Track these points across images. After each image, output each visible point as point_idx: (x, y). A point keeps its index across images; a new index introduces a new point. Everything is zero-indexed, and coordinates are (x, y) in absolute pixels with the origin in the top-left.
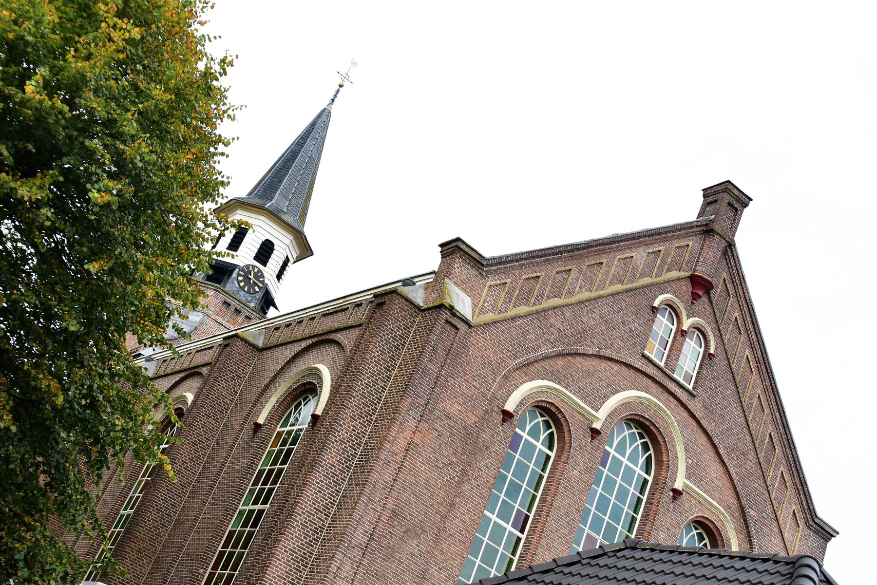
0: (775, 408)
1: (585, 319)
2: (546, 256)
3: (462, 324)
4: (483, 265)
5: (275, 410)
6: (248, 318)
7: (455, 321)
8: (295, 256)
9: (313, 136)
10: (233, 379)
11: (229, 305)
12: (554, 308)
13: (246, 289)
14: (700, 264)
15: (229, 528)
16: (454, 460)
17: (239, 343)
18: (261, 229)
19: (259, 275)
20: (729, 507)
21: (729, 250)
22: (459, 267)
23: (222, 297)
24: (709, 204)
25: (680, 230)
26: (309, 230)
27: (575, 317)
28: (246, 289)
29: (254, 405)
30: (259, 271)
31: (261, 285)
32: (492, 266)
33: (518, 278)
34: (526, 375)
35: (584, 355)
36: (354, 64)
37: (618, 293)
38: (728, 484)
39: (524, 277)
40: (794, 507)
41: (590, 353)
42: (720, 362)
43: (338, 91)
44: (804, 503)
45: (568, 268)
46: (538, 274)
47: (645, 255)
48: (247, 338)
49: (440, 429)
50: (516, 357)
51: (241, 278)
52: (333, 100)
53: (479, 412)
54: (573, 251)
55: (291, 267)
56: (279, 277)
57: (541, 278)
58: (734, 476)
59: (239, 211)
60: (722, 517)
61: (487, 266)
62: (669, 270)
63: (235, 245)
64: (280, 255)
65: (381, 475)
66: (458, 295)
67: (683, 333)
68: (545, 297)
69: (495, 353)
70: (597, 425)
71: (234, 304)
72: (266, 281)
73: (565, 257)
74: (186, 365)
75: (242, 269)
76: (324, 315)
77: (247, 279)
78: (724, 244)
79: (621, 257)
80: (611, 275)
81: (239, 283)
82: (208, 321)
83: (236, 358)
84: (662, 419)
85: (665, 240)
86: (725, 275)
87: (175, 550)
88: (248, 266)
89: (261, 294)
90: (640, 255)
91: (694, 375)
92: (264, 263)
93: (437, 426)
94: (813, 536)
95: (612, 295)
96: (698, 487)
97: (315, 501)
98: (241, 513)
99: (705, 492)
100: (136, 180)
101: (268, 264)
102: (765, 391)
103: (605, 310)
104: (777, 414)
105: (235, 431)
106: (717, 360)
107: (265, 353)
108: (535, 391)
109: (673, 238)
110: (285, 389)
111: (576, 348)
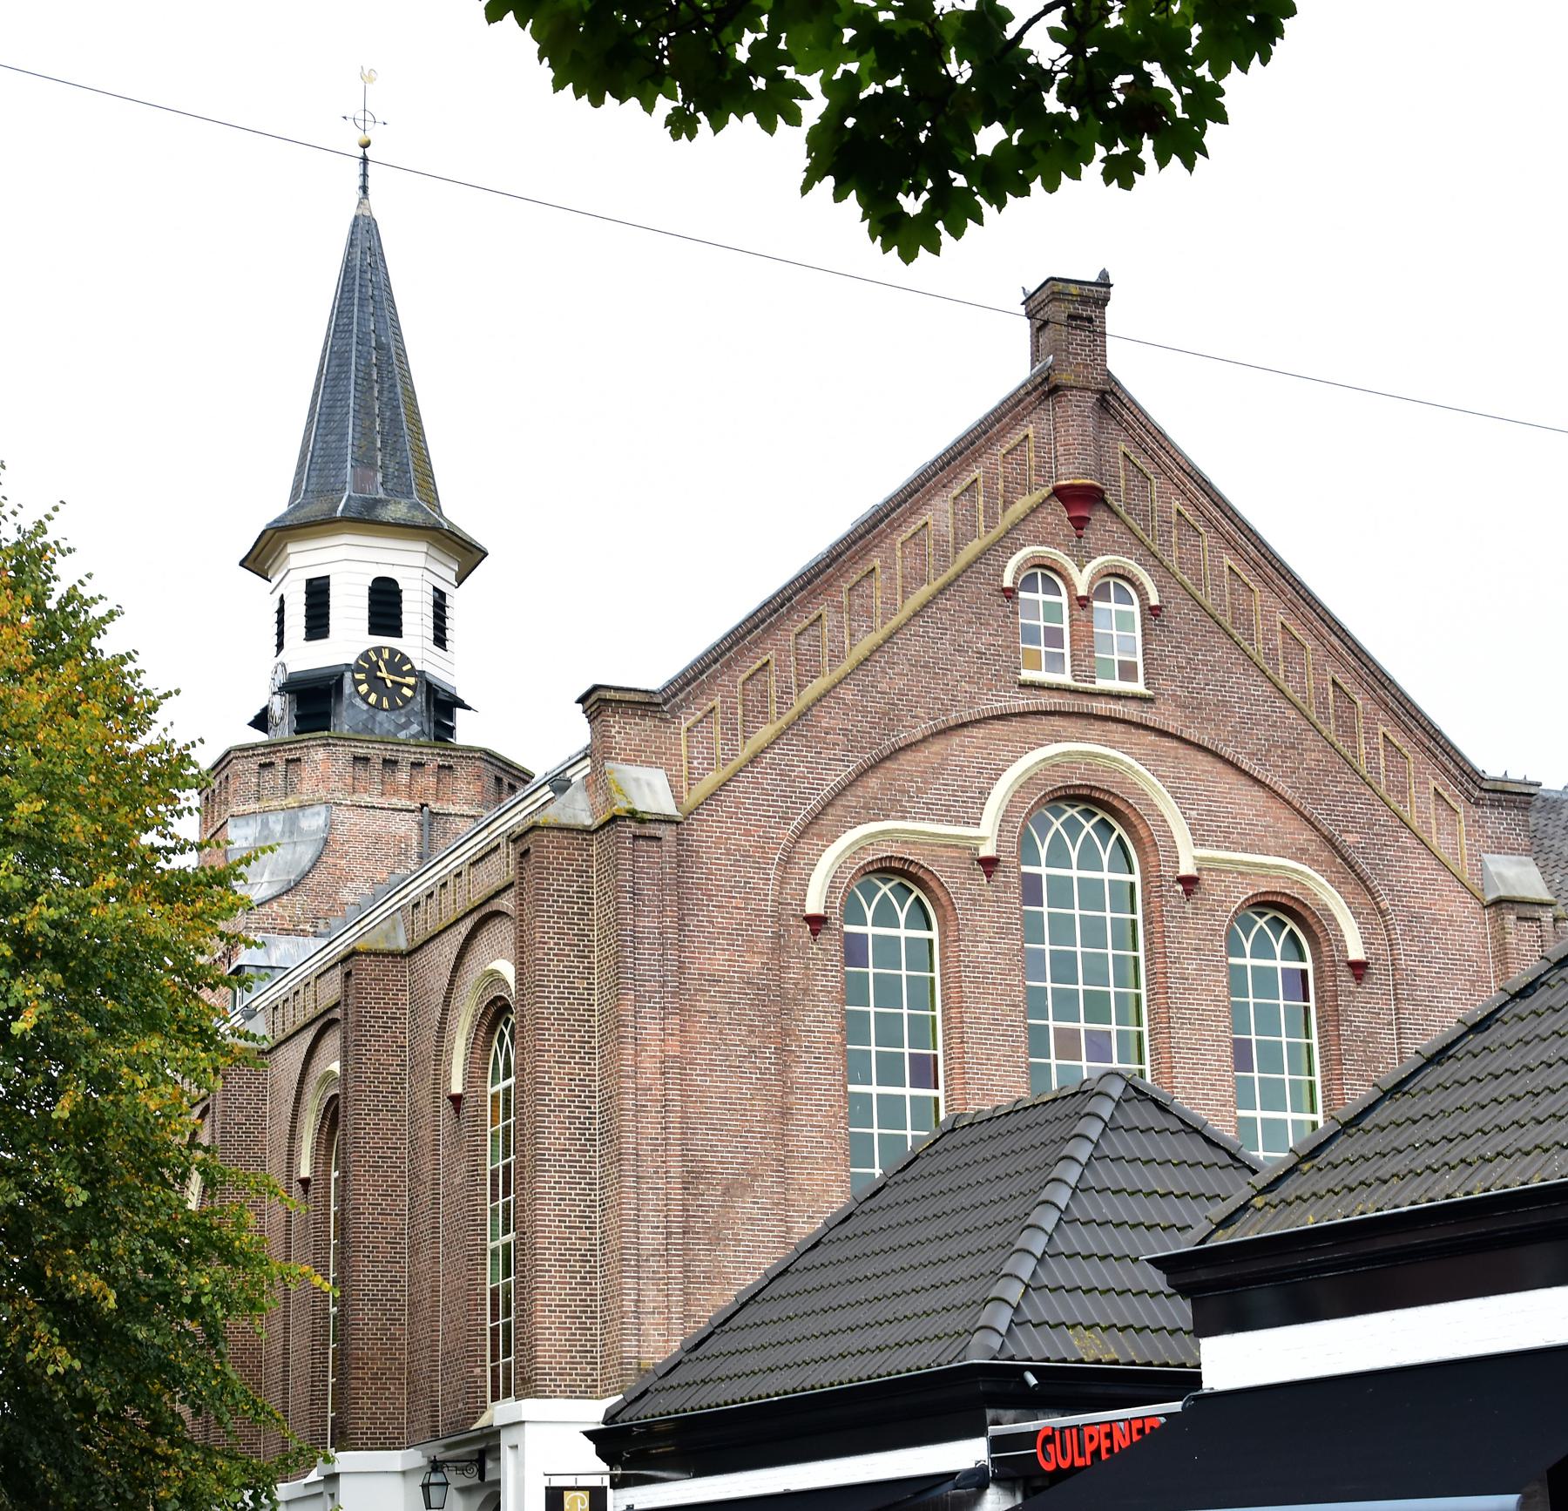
0: (1325, 630)
1: (883, 686)
2: (763, 621)
3: (663, 826)
4: (658, 705)
5: (469, 1061)
6: (417, 765)
7: (650, 830)
8: (451, 577)
10: (386, 1028)
11: (366, 760)
12: (819, 700)
13: (386, 704)
14: (1062, 459)
15: (489, 1286)
16: (755, 1042)
17: (366, 962)
18: (350, 564)
19: (398, 662)
20: (1304, 851)
21: (1110, 400)
22: (623, 730)
23: (344, 752)
24: (1039, 329)
25: (998, 420)
26: (457, 511)
27: (863, 693)
28: (386, 704)
29: (438, 1061)
31: (411, 680)
32: (675, 695)
33: (723, 694)
34: (820, 836)
35: (909, 746)
36: (367, 77)
37: (926, 605)
38: (1286, 813)
39: (740, 680)
40: (1433, 784)
41: (919, 736)
42: (1180, 611)
44: (1451, 766)
45: (813, 617)
46: (765, 659)
47: (949, 506)
48: (374, 947)
49: (708, 1007)
50: (786, 819)
51: (363, 688)
52: (364, 188)
53: (764, 944)
54: (809, 582)
55: (458, 601)
56: (440, 640)
57: (773, 662)
58: (1289, 794)
59: (291, 548)
60: (1295, 877)
61: (666, 702)
62: (1007, 504)
63: (317, 626)
65: (642, 1131)
66: (637, 780)
67: (1083, 602)
68: (795, 690)
69: (747, 833)
70: (987, 851)
71: (376, 752)
72: (418, 668)
73: (798, 603)
74: (311, 1012)
76: (473, 864)
77: (375, 683)
78: (1091, 399)
79: (905, 536)
80: (899, 581)
81: (365, 698)
82: (342, 814)
83: (374, 990)
84: (1108, 770)
85: (977, 456)
86: (1122, 447)
87: (426, 1353)
88: (365, 656)
89: (421, 699)
90: (939, 513)
91: (1139, 659)
92: (396, 631)
93: (702, 1005)
94: (1492, 815)
95: (916, 614)
96: (1227, 849)
97: (562, 1217)
98: (494, 1253)
99: (1245, 851)
100: (59, 957)
101: (405, 629)
102: (1292, 608)
103: (915, 647)
104: (1333, 639)
105: (429, 1118)
106: (1171, 609)
107: (417, 957)
108: (848, 854)
109: (991, 442)
110: (469, 1019)
111: (887, 744)
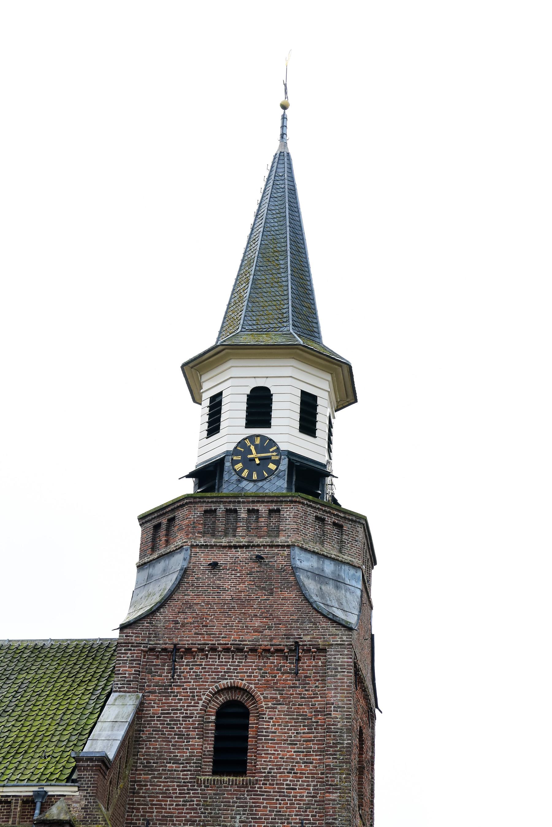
9: (282, 163)
13: (255, 477)
19: (268, 444)
28: (255, 477)
30: (263, 438)
43: (284, 118)
51: (239, 466)
59: (204, 378)
64: (287, 413)
75: (235, 451)
77: (249, 463)
88: (241, 443)
92: (267, 424)
101: (273, 422)
